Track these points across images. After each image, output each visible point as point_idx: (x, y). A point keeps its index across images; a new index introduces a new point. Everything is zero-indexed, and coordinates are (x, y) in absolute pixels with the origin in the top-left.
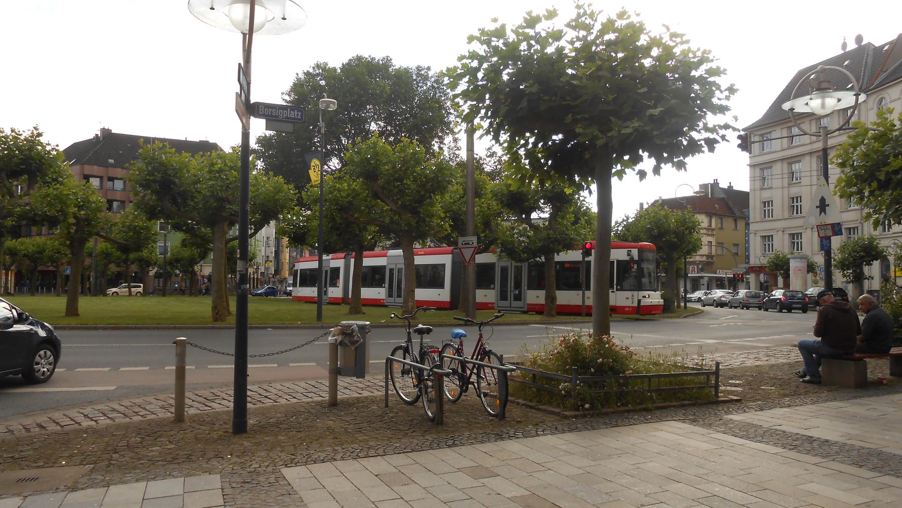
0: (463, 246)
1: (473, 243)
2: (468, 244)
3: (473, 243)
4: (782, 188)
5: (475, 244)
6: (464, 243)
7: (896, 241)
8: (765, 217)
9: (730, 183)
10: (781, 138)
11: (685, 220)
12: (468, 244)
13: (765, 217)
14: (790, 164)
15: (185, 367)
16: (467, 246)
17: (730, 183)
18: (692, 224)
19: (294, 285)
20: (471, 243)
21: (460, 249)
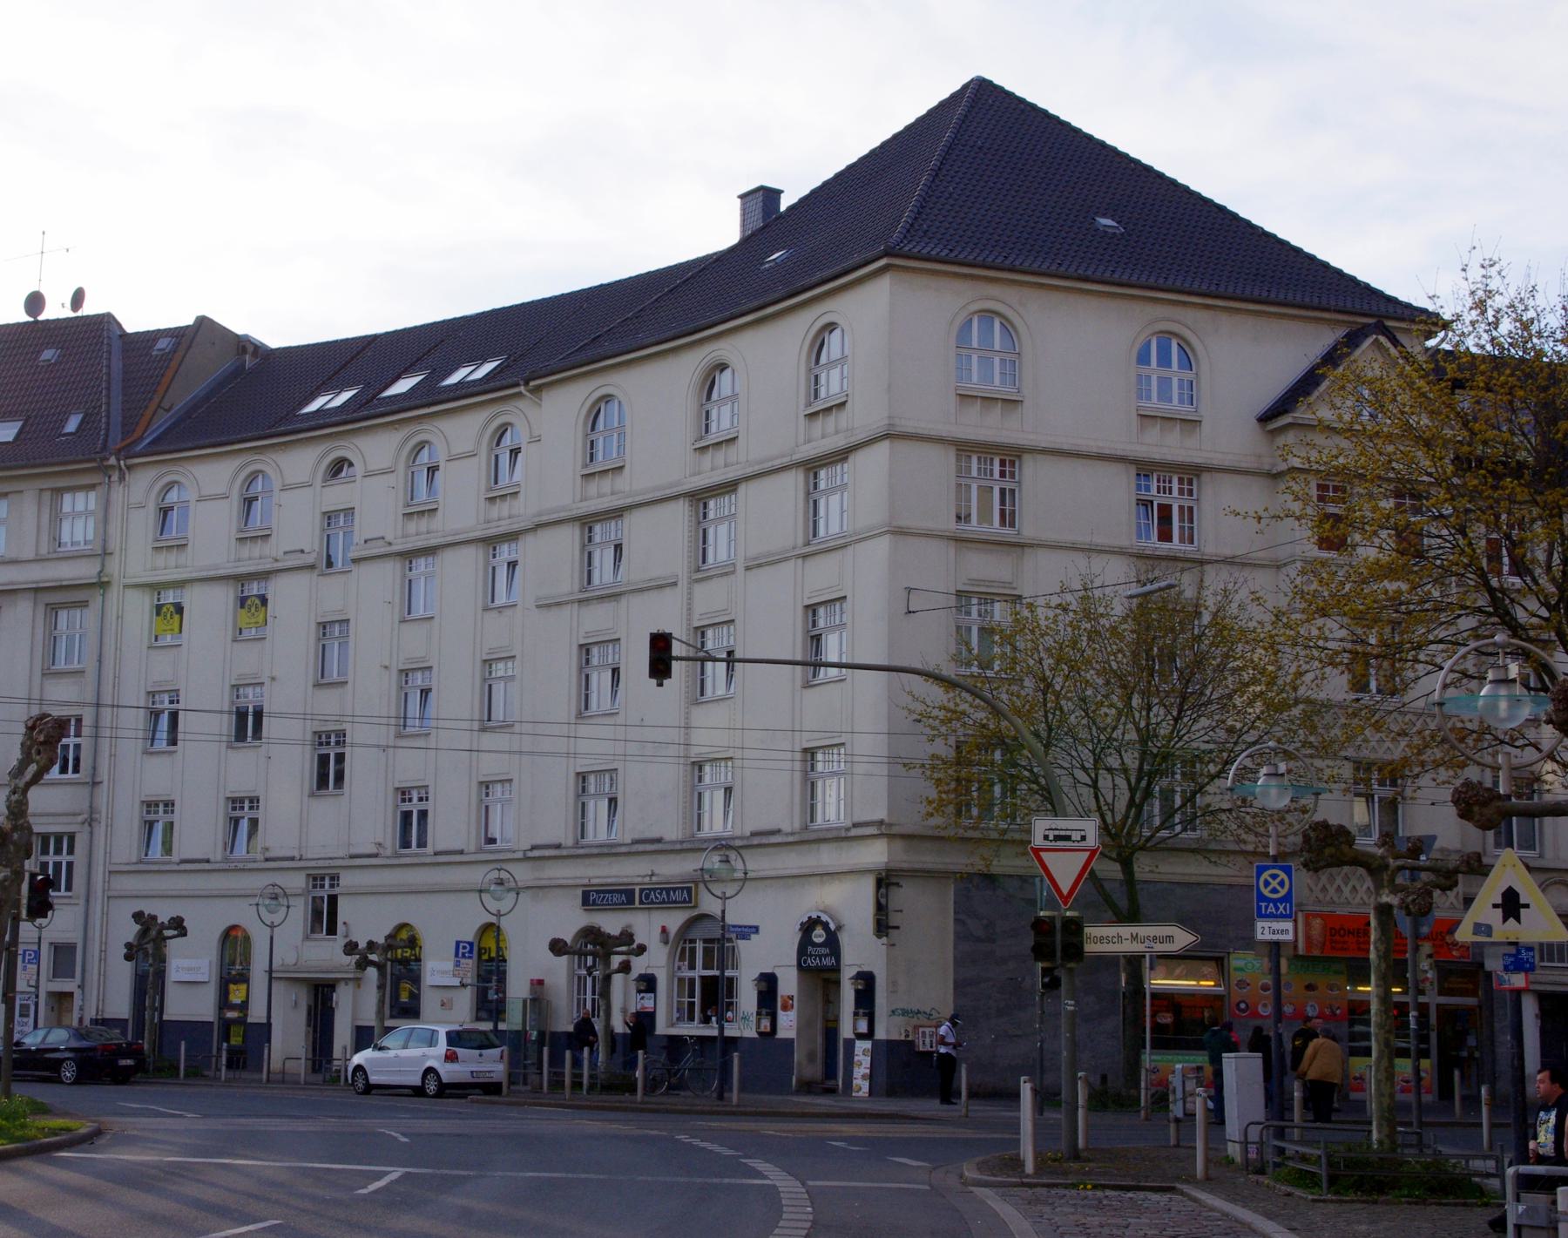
0: (1048, 844)
1: (1083, 838)
2: (1068, 838)
3: (1083, 838)
4: (98, 705)
5: (1092, 841)
6: (1051, 835)
7: (504, 875)
8: (406, 844)
9: (897, 928)
10: (510, 752)
11: (1478, 856)
12: (1068, 838)
13: (406, 844)
14: (53, 609)
15: (1082, 948)
16: (1061, 844)
17: (897, 928)
18: (1441, 779)
19: (1384, 911)
20: (1076, 836)
21: (1037, 851)
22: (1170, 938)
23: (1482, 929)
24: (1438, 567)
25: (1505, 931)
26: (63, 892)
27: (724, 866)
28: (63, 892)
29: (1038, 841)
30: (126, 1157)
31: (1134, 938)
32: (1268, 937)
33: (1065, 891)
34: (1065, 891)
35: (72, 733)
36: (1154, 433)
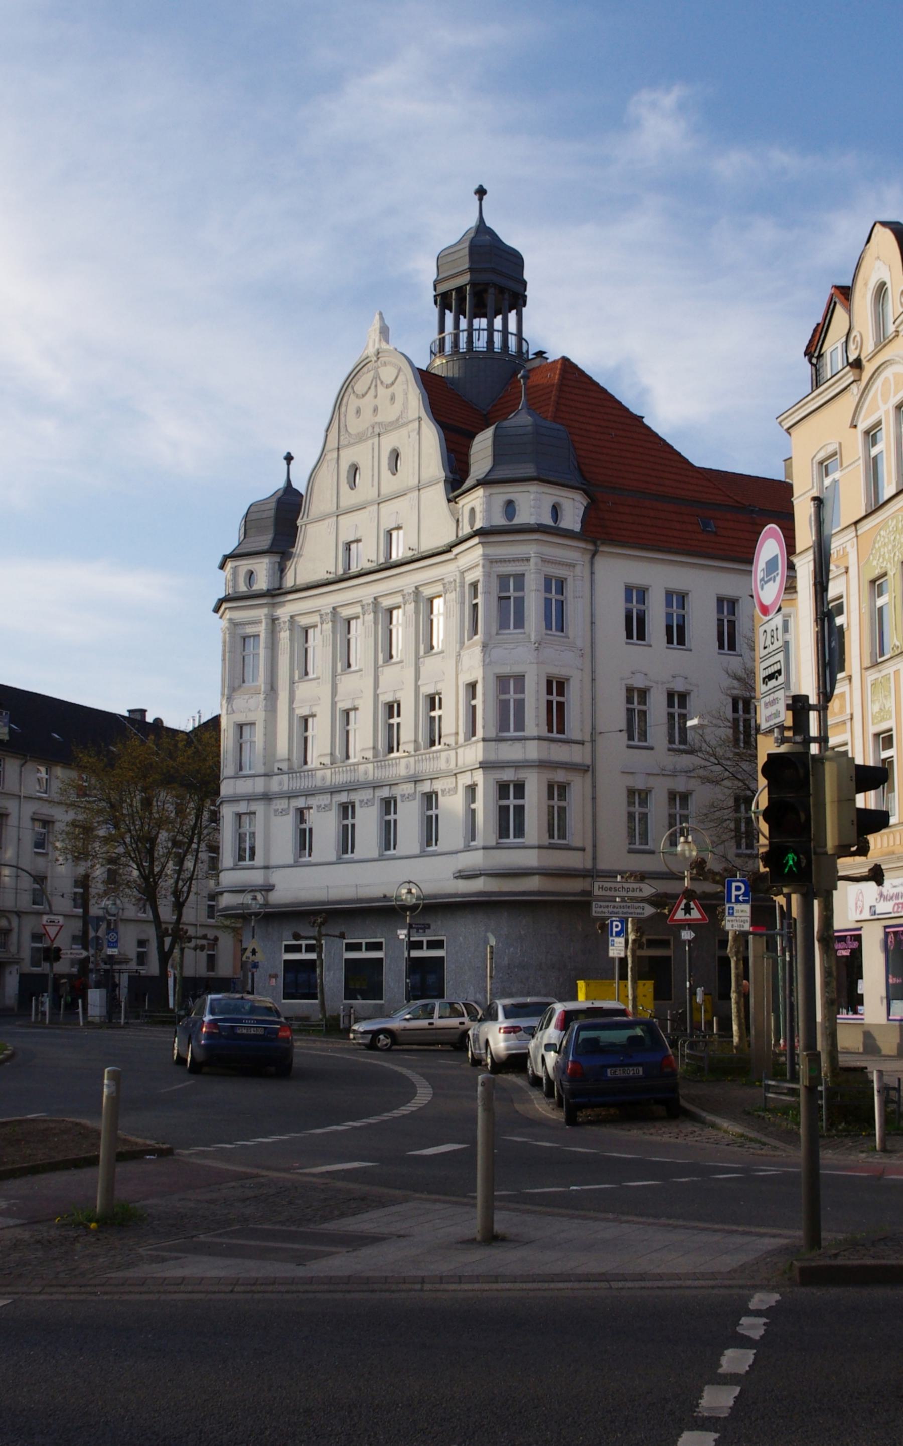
2: (54, 922)
12: (54, 922)
16: (51, 924)
20: (56, 921)
21: (44, 926)
22: (81, 954)
23: (248, 958)
24: (137, 844)
25: (252, 958)
26: (849, 748)
27: (254, 902)
28: (849, 748)
29: (44, 923)
30: (386, 1064)
31: (71, 954)
32: (111, 953)
33: (675, 918)
34: (675, 918)
35: (251, 680)
36: (810, 507)
